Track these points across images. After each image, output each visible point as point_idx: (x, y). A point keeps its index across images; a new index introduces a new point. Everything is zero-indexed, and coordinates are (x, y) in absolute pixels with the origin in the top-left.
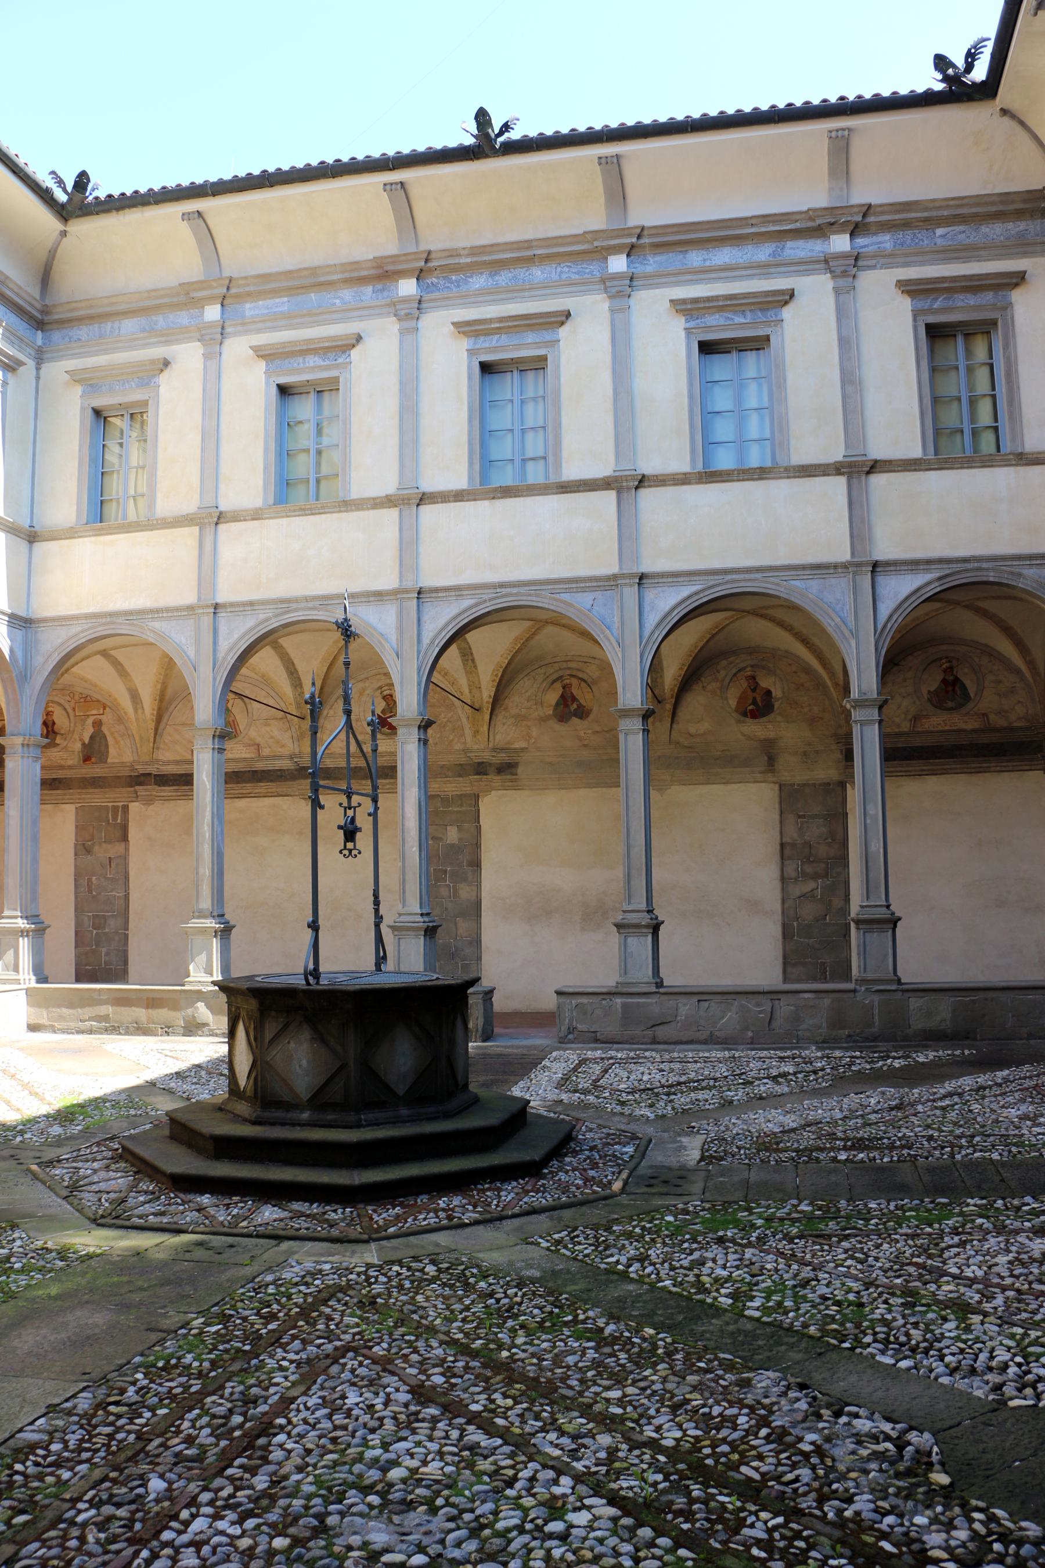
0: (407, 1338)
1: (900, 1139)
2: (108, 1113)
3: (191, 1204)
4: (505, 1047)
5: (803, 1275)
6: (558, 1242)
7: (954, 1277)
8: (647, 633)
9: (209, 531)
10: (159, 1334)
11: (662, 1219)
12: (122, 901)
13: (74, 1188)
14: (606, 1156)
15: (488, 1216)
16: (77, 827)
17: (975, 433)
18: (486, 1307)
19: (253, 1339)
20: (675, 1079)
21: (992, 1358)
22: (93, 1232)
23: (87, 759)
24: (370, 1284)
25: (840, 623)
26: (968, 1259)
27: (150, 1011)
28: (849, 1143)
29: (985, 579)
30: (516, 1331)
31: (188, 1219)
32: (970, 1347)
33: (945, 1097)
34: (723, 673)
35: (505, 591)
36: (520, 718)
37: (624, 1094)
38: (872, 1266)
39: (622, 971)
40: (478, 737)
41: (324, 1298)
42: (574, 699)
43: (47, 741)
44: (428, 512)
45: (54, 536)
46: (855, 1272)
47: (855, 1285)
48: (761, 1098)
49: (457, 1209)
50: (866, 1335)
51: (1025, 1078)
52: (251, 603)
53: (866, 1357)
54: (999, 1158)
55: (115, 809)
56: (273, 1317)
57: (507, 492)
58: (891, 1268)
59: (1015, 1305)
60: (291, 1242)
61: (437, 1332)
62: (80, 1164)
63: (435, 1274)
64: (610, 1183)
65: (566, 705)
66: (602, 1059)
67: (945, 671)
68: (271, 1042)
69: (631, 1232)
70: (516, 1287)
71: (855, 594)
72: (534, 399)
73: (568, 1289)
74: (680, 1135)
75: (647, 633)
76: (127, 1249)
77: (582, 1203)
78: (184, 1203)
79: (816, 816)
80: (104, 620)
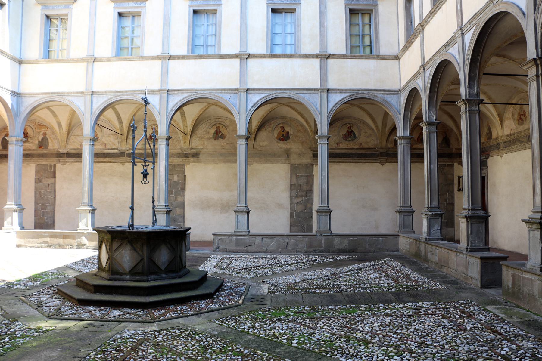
0: (173, 357)
1: (336, 285)
2: (50, 277)
3: (86, 310)
4: (195, 253)
5: (310, 332)
6: (222, 321)
7: (361, 331)
8: (248, 109)
9: (90, 65)
10: (78, 359)
11: (258, 313)
12: (53, 200)
13: (39, 305)
14: (235, 291)
15: (196, 313)
16: (36, 172)
17: (364, 47)
18: (200, 345)
19: (115, 359)
20: (256, 265)
21: (378, 358)
22: (48, 321)
23: (40, 147)
24: (156, 338)
25: (315, 109)
26: (365, 325)
27: (64, 240)
28: (319, 287)
29: (365, 97)
30: (212, 353)
31: (85, 315)
32: (370, 354)
33: (348, 271)
34: (273, 125)
35: (199, 92)
36: (201, 138)
37: (238, 270)
38: (333, 328)
39: (236, 228)
40: (186, 144)
41: (140, 343)
42: (220, 132)
43: (25, 139)
44: (171, 62)
45: (29, 62)
46: (328, 330)
47: (328, 335)
48: (286, 271)
49: (185, 310)
50: (335, 351)
51: (374, 265)
52: (106, 92)
53: (336, 359)
54: (370, 291)
55: (51, 166)
56: (121, 351)
57: (201, 57)
58: (339, 329)
59: (383, 340)
60: (125, 323)
61: (183, 354)
62: (41, 296)
63: (180, 333)
64: (238, 300)
65: (217, 134)
66: (229, 258)
67: (348, 128)
68: (115, 250)
69: (248, 318)
70: (210, 338)
71: (321, 99)
72: (212, 24)
73: (228, 338)
74: (260, 284)
75: (248, 109)
76: (62, 327)
77: (229, 308)
78: (83, 309)
79: (302, 176)
80: (49, 95)
